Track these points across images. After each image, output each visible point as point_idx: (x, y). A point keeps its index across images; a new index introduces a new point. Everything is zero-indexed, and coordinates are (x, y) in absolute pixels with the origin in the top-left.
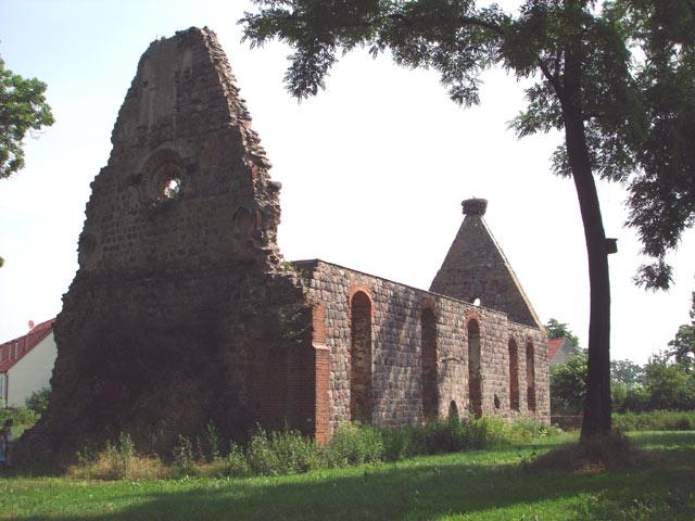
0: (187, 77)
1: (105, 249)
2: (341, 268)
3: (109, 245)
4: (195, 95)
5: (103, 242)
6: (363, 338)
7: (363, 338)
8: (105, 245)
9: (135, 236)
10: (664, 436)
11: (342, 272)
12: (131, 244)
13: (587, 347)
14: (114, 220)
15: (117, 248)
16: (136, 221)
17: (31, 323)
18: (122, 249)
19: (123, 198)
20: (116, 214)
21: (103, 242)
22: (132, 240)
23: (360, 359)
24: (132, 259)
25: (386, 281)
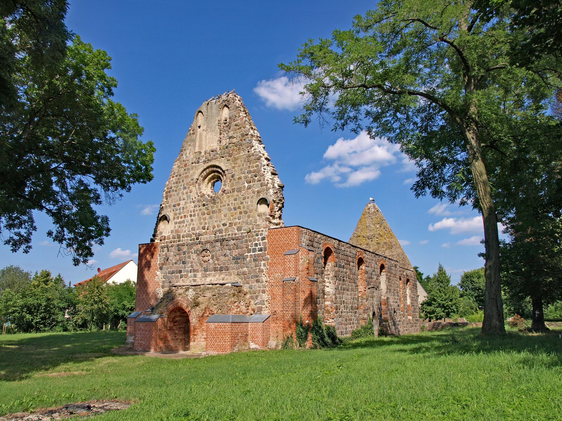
0: (225, 123)
1: (176, 223)
2: (319, 233)
3: (178, 221)
4: (231, 134)
5: (174, 219)
6: (329, 274)
7: (329, 274)
8: (176, 220)
9: (194, 215)
10: (538, 336)
11: (319, 236)
12: (192, 220)
13: (136, 281)
14: (181, 206)
15: (183, 222)
16: (195, 206)
17: (481, 255)
18: (186, 223)
19: (187, 193)
20: (182, 203)
21: (174, 219)
22: (192, 218)
23: (328, 287)
24: (193, 229)
25: (340, 241)
